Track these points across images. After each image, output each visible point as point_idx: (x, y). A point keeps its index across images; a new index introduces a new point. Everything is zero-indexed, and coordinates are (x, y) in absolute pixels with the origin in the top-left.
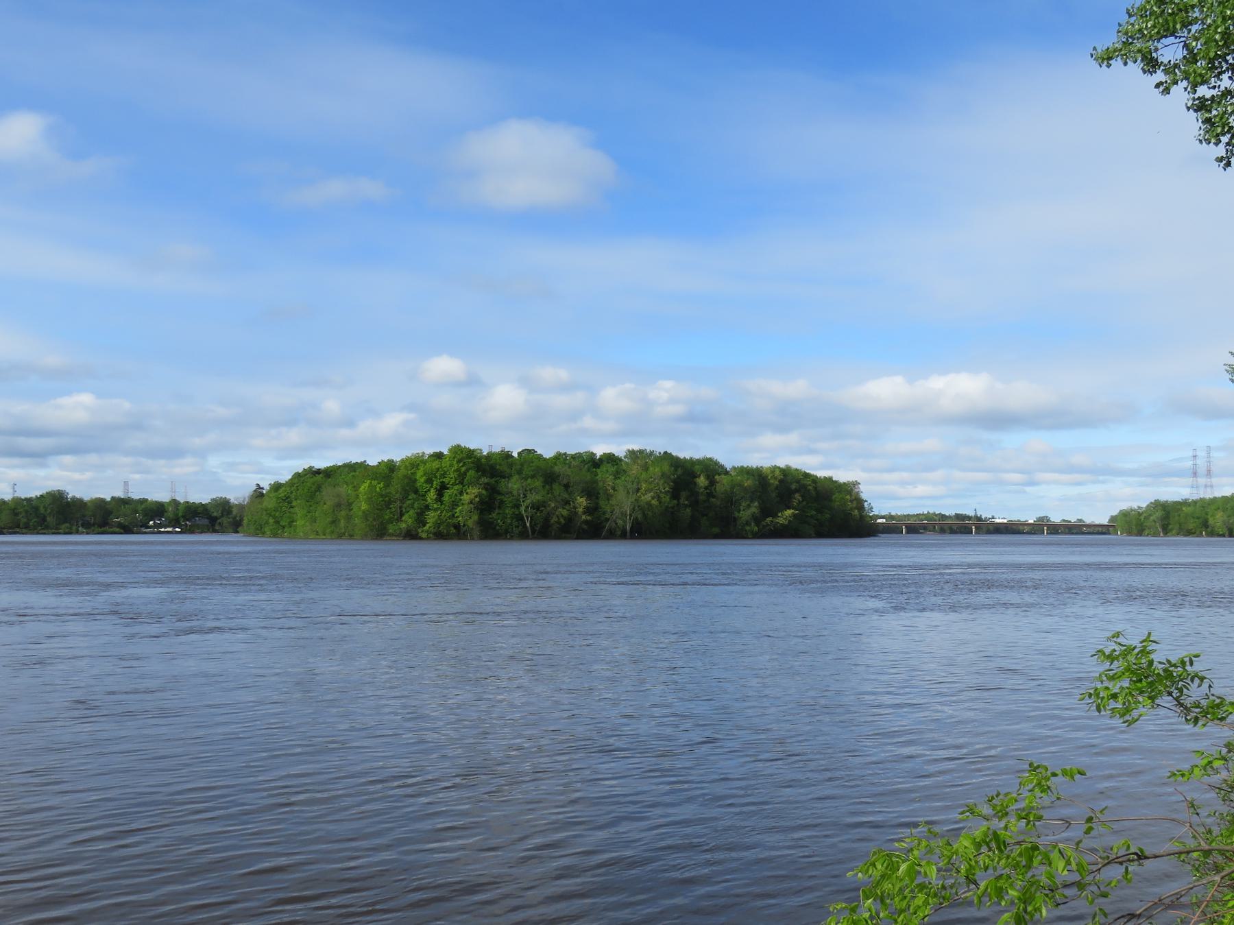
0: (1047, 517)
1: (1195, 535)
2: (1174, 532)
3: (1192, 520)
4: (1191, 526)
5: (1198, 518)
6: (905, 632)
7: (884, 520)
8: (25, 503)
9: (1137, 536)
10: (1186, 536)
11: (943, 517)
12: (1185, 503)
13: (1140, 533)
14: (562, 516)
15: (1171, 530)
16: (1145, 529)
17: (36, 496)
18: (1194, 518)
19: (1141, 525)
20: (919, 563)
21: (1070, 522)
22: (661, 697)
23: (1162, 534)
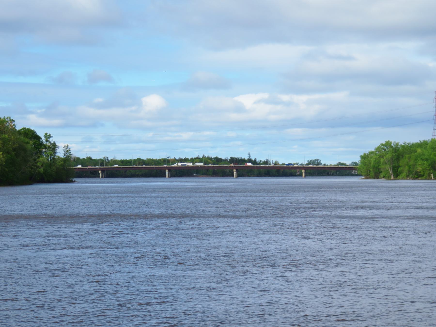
0: (318, 160)
1: (424, 177)
2: (404, 174)
3: (420, 162)
4: (419, 168)
5: (427, 160)
6: (335, 264)
7: (202, 164)
8: (182, 161)
9: (374, 178)
10: (415, 178)
11: (218, 160)
12: (423, 145)
13: (377, 176)
14: (379, 165)
15: (400, 173)
16: (381, 172)
17: (204, 156)
18: (423, 160)
19: (377, 168)
20: (34, 214)
21: (345, 164)
22: (378, 299)
23: (392, 178)
